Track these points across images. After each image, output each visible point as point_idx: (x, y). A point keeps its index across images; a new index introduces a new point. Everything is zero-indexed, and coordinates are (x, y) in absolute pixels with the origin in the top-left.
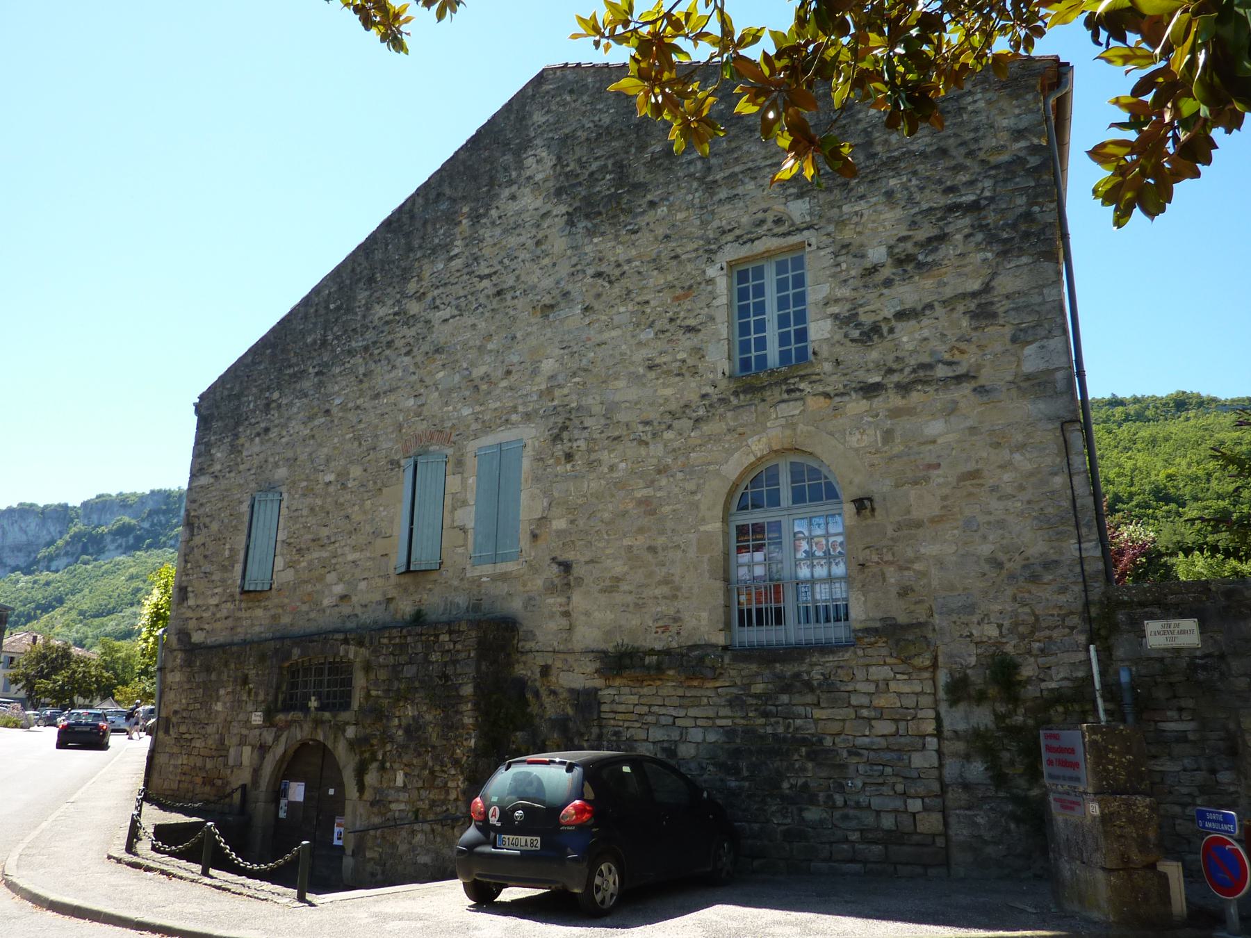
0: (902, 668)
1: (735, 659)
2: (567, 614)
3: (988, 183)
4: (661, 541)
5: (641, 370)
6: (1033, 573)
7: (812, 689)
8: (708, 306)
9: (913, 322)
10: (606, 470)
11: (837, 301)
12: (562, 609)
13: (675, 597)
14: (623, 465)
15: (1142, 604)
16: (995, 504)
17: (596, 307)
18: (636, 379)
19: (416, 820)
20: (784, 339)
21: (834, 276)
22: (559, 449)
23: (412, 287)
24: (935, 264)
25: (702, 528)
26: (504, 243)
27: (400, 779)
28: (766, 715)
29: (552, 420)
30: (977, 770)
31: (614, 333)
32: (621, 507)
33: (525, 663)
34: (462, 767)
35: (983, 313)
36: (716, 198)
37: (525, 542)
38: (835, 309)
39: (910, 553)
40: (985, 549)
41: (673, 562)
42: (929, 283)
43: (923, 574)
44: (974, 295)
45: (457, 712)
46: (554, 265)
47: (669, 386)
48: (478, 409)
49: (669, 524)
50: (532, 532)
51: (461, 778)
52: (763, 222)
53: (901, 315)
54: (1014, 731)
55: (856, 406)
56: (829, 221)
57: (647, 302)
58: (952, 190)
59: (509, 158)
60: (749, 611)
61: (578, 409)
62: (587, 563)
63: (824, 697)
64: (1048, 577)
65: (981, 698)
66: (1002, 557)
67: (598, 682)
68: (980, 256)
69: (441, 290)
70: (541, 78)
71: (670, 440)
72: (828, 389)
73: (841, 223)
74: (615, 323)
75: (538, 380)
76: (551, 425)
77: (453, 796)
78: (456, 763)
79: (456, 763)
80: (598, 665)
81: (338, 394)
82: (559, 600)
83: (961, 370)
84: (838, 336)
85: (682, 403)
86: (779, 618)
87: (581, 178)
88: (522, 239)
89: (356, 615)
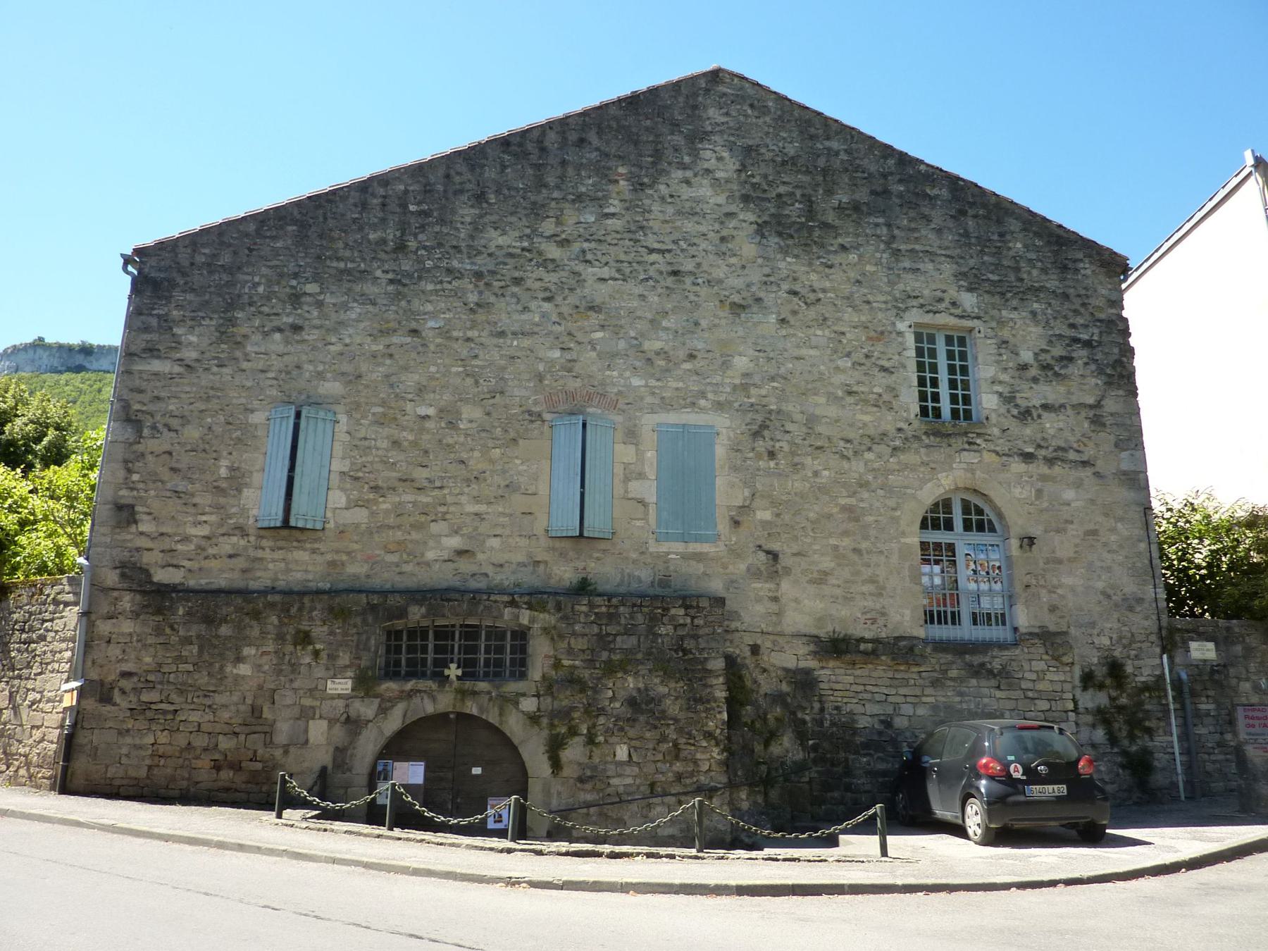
0: (1053, 663)
1: (935, 650)
2: (775, 599)
3: (1096, 331)
4: (864, 545)
5: (840, 393)
6: (1131, 604)
7: (995, 676)
8: (899, 354)
9: (1053, 415)
10: (810, 474)
11: (1000, 382)
12: (770, 594)
13: (881, 595)
14: (826, 473)
15: (1188, 631)
16: (1105, 555)
17: (792, 323)
18: (833, 399)
19: (653, 793)
20: (954, 399)
21: (998, 362)
22: (761, 445)
23: (548, 227)
24: (1065, 377)
25: (903, 540)
26: (678, 223)
27: (622, 752)
28: (961, 694)
29: (750, 415)
30: (1100, 734)
31: (812, 352)
32: (826, 510)
33: (731, 642)
34: (715, 738)
35: (1097, 422)
36: (901, 265)
37: (723, 527)
38: (999, 388)
39: (1055, 582)
40: (1100, 585)
41: (878, 565)
42: (1062, 389)
43: (1063, 597)
44: (1091, 407)
45: (705, 686)
46: (744, 267)
47: (867, 413)
48: (653, 382)
49: (873, 533)
50: (732, 518)
51: (716, 750)
52: (941, 300)
53: (1045, 407)
54: (1121, 709)
55: (1017, 466)
56: (992, 318)
57: (843, 333)
58: (1072, 326)
59: (678, 139)
60: (945, 612)
61: (779, 412)
62: (794, 555)
63: (1003, 681)
64: (1138, 609)
65: (1101, 687)
66: (1111, 592)
67: (811, 663)
68: (1093, 381)
69: (593, 245)
70: (716, 76)
71: (871, 461)
72: (998, 449)
73: (1001, 323)
74: (813, 343)
75: (729, 373)
76: (748, 420)
77: (705, 767)
78: (709, 735)
79: (709, 735)
80: (812, 647)
81: (433, 315)
82: (767, 585)
83: (1085, 458)
84: (1003, 410)
85: (880, 431)
86: (955, 619)
87: (768, 195)
88: (703, 229)
89: (486, 575)
